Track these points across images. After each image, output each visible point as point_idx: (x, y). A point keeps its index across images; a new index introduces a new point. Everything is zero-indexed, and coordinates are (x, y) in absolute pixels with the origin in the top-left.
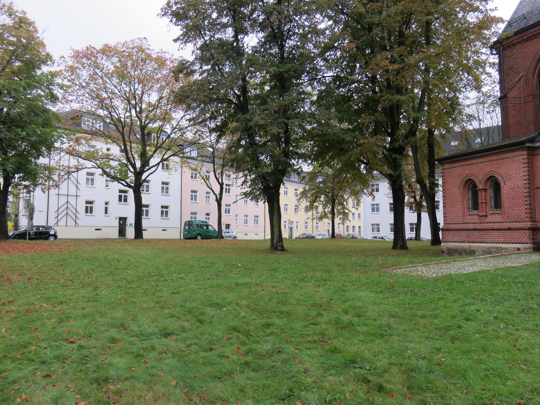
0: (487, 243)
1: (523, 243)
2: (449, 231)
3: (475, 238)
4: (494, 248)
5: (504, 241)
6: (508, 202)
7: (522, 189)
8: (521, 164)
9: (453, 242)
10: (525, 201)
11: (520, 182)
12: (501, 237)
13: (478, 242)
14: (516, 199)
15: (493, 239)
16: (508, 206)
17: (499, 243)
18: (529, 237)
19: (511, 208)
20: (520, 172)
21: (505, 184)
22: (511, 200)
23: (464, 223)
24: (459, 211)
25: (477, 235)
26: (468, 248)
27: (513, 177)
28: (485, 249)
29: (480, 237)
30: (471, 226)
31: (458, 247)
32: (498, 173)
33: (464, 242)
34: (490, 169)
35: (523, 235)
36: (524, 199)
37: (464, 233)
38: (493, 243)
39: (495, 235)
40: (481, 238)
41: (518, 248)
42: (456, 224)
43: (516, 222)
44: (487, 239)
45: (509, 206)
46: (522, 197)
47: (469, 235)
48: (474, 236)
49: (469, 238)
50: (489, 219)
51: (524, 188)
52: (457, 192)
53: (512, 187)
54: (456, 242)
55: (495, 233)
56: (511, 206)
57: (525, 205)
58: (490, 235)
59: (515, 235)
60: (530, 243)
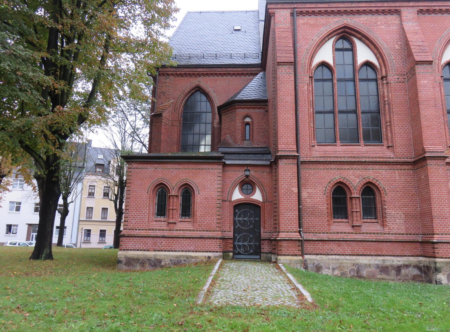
1: (214, 252)
3: (161, 246)
4: (183, 256)
9: (134, 250)
11: (214, 194)
12: (192, 245)
13: (165, 251)
14: (209, 209)
17: (189, 251)
19: (203, 217)
21: (199, 194)
23: (149, 230)
24: (145, 216)
26: (153, 257)
28: (174, 257)
30: (158, 233)
31: (141, 256)
33: (148, 250)
34: (186, 176)
35: (213, 243)
37: (150, 241)
39: (186, 243)
42: (139, 230)
43: (207, 231)
44: (176, 247)
48: (161, 244)
50: (179, 226)
58: (180, 243)
60: (220, 252)
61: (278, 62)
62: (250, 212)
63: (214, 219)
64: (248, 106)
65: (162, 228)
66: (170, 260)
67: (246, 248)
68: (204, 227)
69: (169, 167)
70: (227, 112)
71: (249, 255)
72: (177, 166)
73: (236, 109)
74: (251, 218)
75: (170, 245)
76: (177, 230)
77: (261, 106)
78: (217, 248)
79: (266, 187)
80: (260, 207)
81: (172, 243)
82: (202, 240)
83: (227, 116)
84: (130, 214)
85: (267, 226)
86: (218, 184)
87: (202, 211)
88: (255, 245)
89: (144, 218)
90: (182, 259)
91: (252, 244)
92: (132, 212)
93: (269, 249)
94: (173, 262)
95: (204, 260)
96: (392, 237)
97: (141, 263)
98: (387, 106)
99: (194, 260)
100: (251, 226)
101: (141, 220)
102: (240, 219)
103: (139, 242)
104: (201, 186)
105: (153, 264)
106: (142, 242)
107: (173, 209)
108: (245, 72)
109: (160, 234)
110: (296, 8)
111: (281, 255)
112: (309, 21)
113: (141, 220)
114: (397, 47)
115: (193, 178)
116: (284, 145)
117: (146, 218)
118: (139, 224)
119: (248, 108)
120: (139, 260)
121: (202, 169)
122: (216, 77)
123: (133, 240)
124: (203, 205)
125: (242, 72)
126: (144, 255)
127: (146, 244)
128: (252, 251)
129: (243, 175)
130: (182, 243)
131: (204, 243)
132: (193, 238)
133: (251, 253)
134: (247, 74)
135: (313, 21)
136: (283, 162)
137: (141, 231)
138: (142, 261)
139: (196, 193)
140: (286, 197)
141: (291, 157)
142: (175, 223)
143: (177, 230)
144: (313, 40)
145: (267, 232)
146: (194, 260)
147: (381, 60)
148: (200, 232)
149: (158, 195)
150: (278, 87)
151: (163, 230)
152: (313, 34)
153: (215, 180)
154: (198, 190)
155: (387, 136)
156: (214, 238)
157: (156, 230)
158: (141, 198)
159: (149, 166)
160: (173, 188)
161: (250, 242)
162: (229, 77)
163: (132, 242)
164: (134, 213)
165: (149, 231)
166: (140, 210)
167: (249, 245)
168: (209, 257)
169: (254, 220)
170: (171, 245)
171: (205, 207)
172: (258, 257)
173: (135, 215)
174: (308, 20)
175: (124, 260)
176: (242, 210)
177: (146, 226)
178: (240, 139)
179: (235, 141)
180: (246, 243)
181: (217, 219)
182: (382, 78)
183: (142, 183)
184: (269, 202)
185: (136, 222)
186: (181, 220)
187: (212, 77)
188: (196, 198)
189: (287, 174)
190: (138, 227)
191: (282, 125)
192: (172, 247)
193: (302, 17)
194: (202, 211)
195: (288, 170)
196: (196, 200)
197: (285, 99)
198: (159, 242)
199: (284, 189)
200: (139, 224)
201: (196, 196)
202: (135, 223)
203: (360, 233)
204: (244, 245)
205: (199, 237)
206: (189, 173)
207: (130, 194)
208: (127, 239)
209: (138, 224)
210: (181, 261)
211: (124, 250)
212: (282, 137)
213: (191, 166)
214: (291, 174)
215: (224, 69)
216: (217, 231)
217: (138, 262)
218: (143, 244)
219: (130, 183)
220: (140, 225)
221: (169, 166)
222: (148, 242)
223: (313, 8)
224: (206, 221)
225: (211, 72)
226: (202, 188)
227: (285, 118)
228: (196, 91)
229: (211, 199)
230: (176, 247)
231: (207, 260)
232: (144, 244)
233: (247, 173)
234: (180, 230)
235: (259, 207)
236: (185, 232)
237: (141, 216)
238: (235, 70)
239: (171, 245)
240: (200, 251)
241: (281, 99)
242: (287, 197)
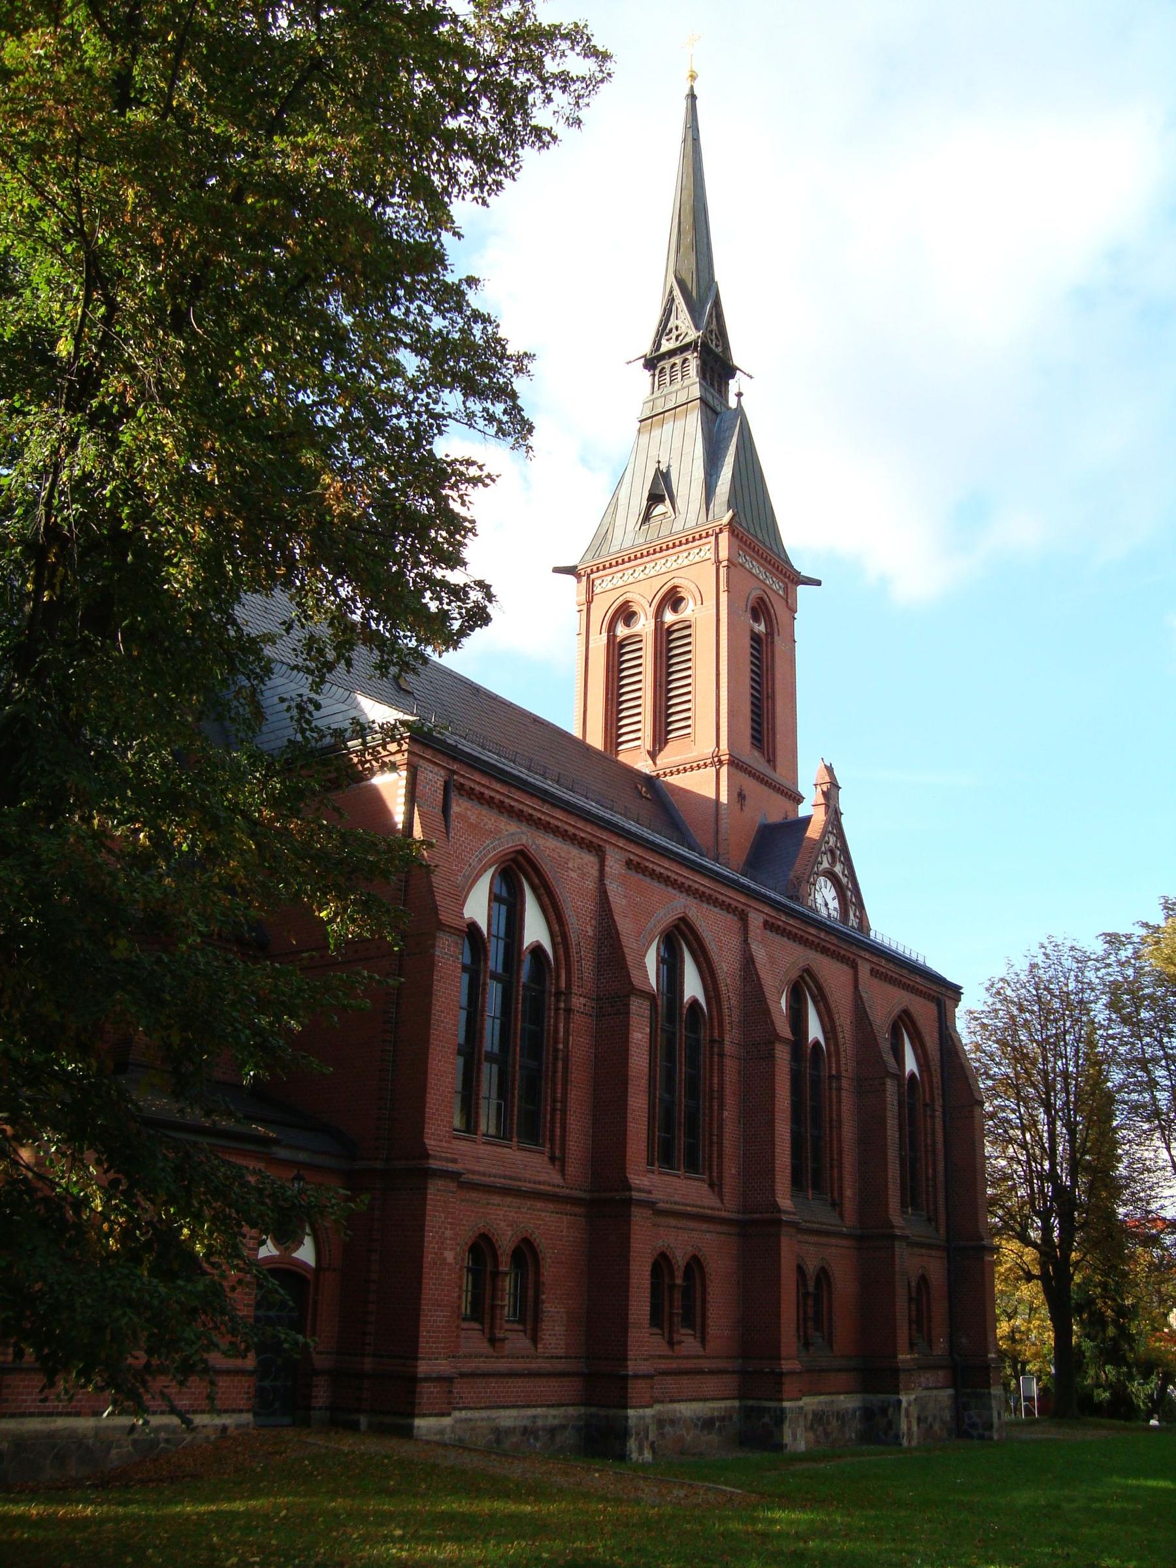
5: (192, 1406)
96: (546, 1366)
98: (560, 1064)
112: (469, 813)
114: (590, 933)
147: (561, 951)
155: (553, 1131)
168: (225, 1428)
174: (467, 809)
182: (558, 994)
203: (502, 1357)
223: (483, 786)
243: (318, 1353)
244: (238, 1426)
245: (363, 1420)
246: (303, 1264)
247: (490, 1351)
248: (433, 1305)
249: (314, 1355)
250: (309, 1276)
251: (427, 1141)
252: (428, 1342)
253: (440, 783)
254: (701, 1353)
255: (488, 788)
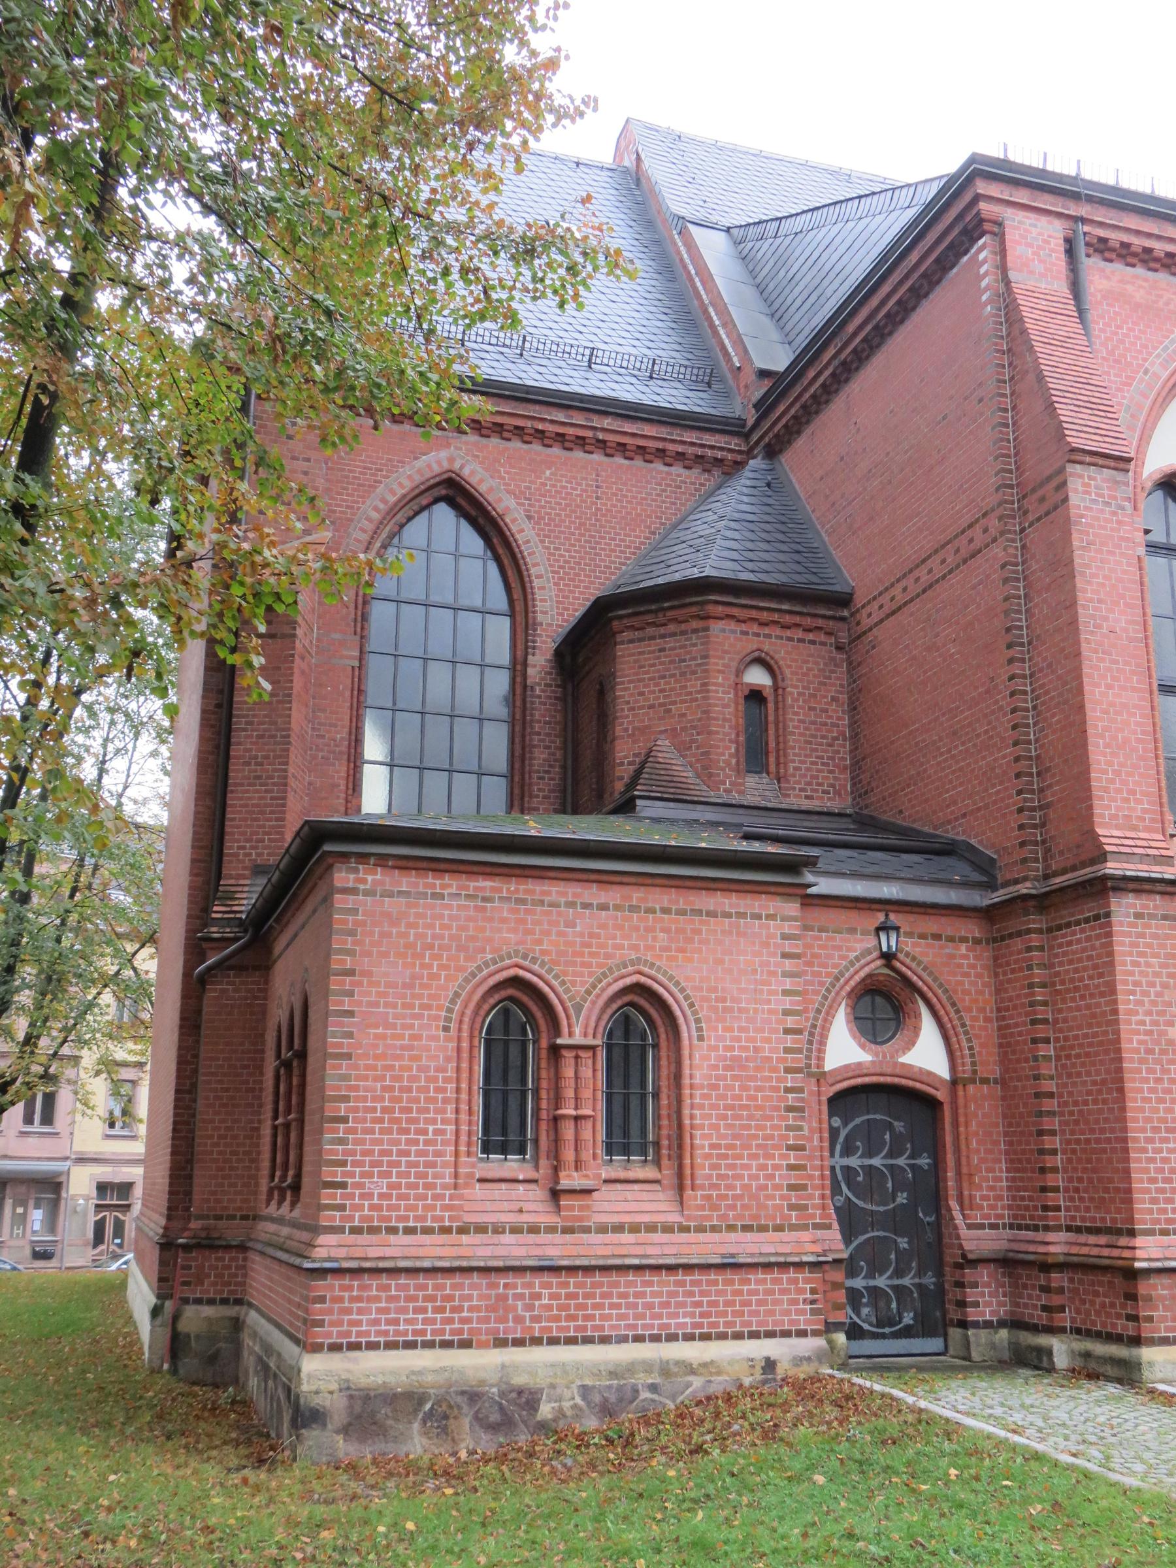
0: (605, 1340)
1: (786, 1334)
2: (366, 1279)
3: (535, 1319)
4: (647, 1366)
5: (695, 1325)
6: (711, 1126)
7: (774, 1070)
8: (774, 955)
9: (391, 1346)
10: (788, 1128)
11: (768, 1040)
12: (683, 1305)
13: (554, 1341)
14: (750, 1117)
15: (642, 1316)
16: (712, 1146)
17: (672, 1338)
18: (813, 1302)
19: (726, 1157)
20: (770, 993)
21: (701, 1038)
22: (725, 1117)
23: (462, 1230)
24: (437, 1154)
25: (552, 1297)
26: (493, 1378)
27: (740, 1010)
28: (598, 1375)
29: (566, 1307)
30: (511, 1248)
31: (430, 1378)
32: (671, 978)
33: (466, 1344)
34: (635, 948)
35: (783, 1292)
36: (786, 1119)
37: (474, 1290)
38: (638, 1339)
39: (654, 1295)
40: (573, 1318)
41: (768, 1359)
42: (409, 1231)
43: (746, 1228)
44: (608, 1317)
45: (718, 1146)
46: (777, 1109)
47: (505, 1298)
48: (530, 1308)
49: (504, 1320)
50: (606, 1207)
51: (787, 1070)
52: (435, 1038)
53: (733, 1058)
54: (410, 1345)
55: (650, 1284)
56: (728, 1147)
57: (789, 1148)
58: (624, 1296)
59: (751, 1293)
60: (816, 1333)
61: (1073, 450)
62: (890, 1126)
63: (776, 1167)
64: (765, 616)
65: (526, 1218)
66: (585, 1391)
67: (882, 1304)
68: (733, 1207)
69: (554, 898)
70: (651, 631)
71: (896, 1335)
72: (593, 894)
73: (707, 617)
74: (900, 1155)
75: (580, 1307)
76: (602, 1229)
77: (776, 617)
78: (803, 1312)
79: (970, 1010)
80: (941, 1103)
81: (587, 1296)
82: (729, 1275)
83: (654, 645)
84: (357, 1142)
85: (983, 1198)
86: (785, 993)
87: (716, 1127)
88: (919, 1286)
89: (433, 1165)
90: (642, 1379)
91: (906, 1281)
92: (367, 1131)
93: (1000, 1304)
94: (597, 1399)
95: (747, 1381)
97: (430, 1415)
99: (697, 1382)
100: (902, 1198)
101: (419, 1175)
102: (854, 1162)
103: (414, 1299)
104: (708, 1000)
105: (495, 1417)
106: (432, 1299)
107: (577, 1118)
108: (671, 447)
109: (522, 1251)
110: (1084, 220)
111: (1152, 1342)
113: (419, 1175)
115: (670, 959)
116: (1117, 827)
117: (445, 1165)
118: (405, 1197)
119: (763, 624)
120: (421, 1399)
121: (709, 914)
122: (537, 447)
123: (381, 1288)
124: (724, 1097)
125: (660, 445)
126: (444, 1369)
127: (454, 1310)
128: (908, 1319)
129: (869, 952)
130: (637, 1295)
131: (739, 1293)
132: (688, 1268)
133: (908, 1327)
134: (680, 456)
135: (1142, 292)
136: (1129, 906)
137: (420, 1238)
138: (438, 1403)
139: (685, 1034)
140: (1149, 1071)
141: (1159, 887)
142: (588, 1192)
143: (602, 1229)
144: (1146, 372)
145: (981, 1227)
146: (697, 1382)
148: (716, 1237)
149: (488, 1043)
150: (1077, 561)
151: (534, 1229)
152: (1145, 346)
153: (773, 974)
154: (698, 1021)
156: (784, 1266)
157: (498, 1230)
158: (413, 1058)
159: (450, 884)
160: (578, 1008)
161: (899, 1273)
162: (597, 457)
163: (377, 1299)
164: (379, 1142)
165: (465, 1238)
166: (410, 1121)
167: (897, 1289)
168: (770, 1365)
169: (912, 1166)
170: (583, 1307)
171: (732, 1108)
172: (935, 1344)
173: (383, 1153)
175: (336, 1406)
176: (858, 1121)
177: (445, 1208)
178: (728, 763)
179: (707, 772)
180: (881, 1282)
181: (791, 1167)
183: (413, 977)
184: (985, 1081)
185: (391, 1186)
186: (613, 1175)
187: (516, 444)
188: (686, 1062)
189: (1148, 965)
190: (400, 1219)
191: (1102, 737)
192: (586, 1318)
193: (1103, 264)
194: (716, 1127)
195: (1150, 946)
196: (686, 1071)
197: (1106, 619)
198: (520, 1297)
199: (1138, 1033)
200: (405, 1197)
201: (686, 1052)
202: (388, 1196)
204: (875, 1287)
205: (717, 1260)
206: (648, 930)
207: (350, 1035)
208: (350, 1288)
209: (400, 1197)
210: (636, 1391)
211: (335, 1348)
212: (1106, 789)
213: (660, 898)
214: (1162, 966)
215: (579, 419)
216: (793, 1228)
217: (416, 1411)
218: (437, 1310)
219: (351, 973)
220: (414, 1208)
221: (554, 891)
222: (463, 1298)
223: (1149, 235)
224: (741, 1177)
225: (520, 423)
226: (715, 1009)
227: (1113, 704)
228: (436, 501)
229: (757, 1069)
230: (608, 1317)
231: (758, 1376)
232: (441, 1310)
233: (888, 942)
234: (619, 1228)
235: (930, 1104)
236: (643, 1236)
237: (420, 1153)
238: (629, 427)
239: (583, 1307)
240: (722, 1336)
241: (1093, 616)
242: (1153, 1071)
243: (970, 1227)
244: (798, 1361)
245: (1061, 1350)
246: (928, 1076)
247: (546, 1218)
248: (1155, 1130)
249: (964, 1232)
250: (940, 1095)
251: (1100, 831)
252: (1154, 1201)
253: (1059, 246)
254: (674, 1218)
255: (1159, 238)
